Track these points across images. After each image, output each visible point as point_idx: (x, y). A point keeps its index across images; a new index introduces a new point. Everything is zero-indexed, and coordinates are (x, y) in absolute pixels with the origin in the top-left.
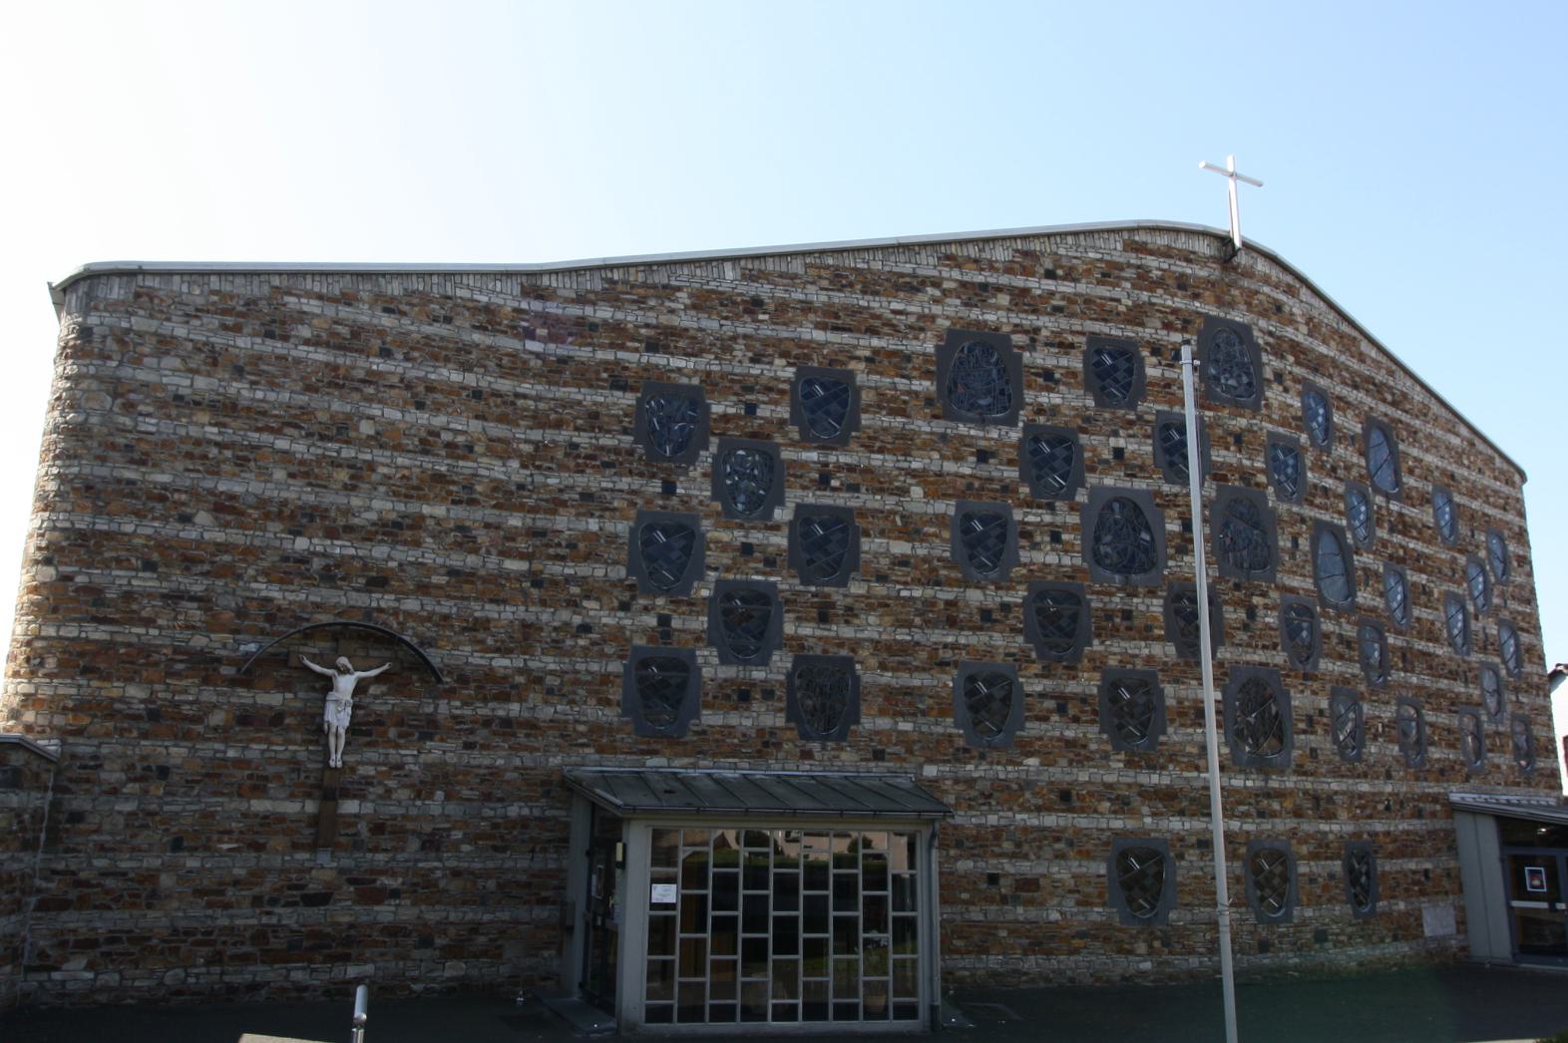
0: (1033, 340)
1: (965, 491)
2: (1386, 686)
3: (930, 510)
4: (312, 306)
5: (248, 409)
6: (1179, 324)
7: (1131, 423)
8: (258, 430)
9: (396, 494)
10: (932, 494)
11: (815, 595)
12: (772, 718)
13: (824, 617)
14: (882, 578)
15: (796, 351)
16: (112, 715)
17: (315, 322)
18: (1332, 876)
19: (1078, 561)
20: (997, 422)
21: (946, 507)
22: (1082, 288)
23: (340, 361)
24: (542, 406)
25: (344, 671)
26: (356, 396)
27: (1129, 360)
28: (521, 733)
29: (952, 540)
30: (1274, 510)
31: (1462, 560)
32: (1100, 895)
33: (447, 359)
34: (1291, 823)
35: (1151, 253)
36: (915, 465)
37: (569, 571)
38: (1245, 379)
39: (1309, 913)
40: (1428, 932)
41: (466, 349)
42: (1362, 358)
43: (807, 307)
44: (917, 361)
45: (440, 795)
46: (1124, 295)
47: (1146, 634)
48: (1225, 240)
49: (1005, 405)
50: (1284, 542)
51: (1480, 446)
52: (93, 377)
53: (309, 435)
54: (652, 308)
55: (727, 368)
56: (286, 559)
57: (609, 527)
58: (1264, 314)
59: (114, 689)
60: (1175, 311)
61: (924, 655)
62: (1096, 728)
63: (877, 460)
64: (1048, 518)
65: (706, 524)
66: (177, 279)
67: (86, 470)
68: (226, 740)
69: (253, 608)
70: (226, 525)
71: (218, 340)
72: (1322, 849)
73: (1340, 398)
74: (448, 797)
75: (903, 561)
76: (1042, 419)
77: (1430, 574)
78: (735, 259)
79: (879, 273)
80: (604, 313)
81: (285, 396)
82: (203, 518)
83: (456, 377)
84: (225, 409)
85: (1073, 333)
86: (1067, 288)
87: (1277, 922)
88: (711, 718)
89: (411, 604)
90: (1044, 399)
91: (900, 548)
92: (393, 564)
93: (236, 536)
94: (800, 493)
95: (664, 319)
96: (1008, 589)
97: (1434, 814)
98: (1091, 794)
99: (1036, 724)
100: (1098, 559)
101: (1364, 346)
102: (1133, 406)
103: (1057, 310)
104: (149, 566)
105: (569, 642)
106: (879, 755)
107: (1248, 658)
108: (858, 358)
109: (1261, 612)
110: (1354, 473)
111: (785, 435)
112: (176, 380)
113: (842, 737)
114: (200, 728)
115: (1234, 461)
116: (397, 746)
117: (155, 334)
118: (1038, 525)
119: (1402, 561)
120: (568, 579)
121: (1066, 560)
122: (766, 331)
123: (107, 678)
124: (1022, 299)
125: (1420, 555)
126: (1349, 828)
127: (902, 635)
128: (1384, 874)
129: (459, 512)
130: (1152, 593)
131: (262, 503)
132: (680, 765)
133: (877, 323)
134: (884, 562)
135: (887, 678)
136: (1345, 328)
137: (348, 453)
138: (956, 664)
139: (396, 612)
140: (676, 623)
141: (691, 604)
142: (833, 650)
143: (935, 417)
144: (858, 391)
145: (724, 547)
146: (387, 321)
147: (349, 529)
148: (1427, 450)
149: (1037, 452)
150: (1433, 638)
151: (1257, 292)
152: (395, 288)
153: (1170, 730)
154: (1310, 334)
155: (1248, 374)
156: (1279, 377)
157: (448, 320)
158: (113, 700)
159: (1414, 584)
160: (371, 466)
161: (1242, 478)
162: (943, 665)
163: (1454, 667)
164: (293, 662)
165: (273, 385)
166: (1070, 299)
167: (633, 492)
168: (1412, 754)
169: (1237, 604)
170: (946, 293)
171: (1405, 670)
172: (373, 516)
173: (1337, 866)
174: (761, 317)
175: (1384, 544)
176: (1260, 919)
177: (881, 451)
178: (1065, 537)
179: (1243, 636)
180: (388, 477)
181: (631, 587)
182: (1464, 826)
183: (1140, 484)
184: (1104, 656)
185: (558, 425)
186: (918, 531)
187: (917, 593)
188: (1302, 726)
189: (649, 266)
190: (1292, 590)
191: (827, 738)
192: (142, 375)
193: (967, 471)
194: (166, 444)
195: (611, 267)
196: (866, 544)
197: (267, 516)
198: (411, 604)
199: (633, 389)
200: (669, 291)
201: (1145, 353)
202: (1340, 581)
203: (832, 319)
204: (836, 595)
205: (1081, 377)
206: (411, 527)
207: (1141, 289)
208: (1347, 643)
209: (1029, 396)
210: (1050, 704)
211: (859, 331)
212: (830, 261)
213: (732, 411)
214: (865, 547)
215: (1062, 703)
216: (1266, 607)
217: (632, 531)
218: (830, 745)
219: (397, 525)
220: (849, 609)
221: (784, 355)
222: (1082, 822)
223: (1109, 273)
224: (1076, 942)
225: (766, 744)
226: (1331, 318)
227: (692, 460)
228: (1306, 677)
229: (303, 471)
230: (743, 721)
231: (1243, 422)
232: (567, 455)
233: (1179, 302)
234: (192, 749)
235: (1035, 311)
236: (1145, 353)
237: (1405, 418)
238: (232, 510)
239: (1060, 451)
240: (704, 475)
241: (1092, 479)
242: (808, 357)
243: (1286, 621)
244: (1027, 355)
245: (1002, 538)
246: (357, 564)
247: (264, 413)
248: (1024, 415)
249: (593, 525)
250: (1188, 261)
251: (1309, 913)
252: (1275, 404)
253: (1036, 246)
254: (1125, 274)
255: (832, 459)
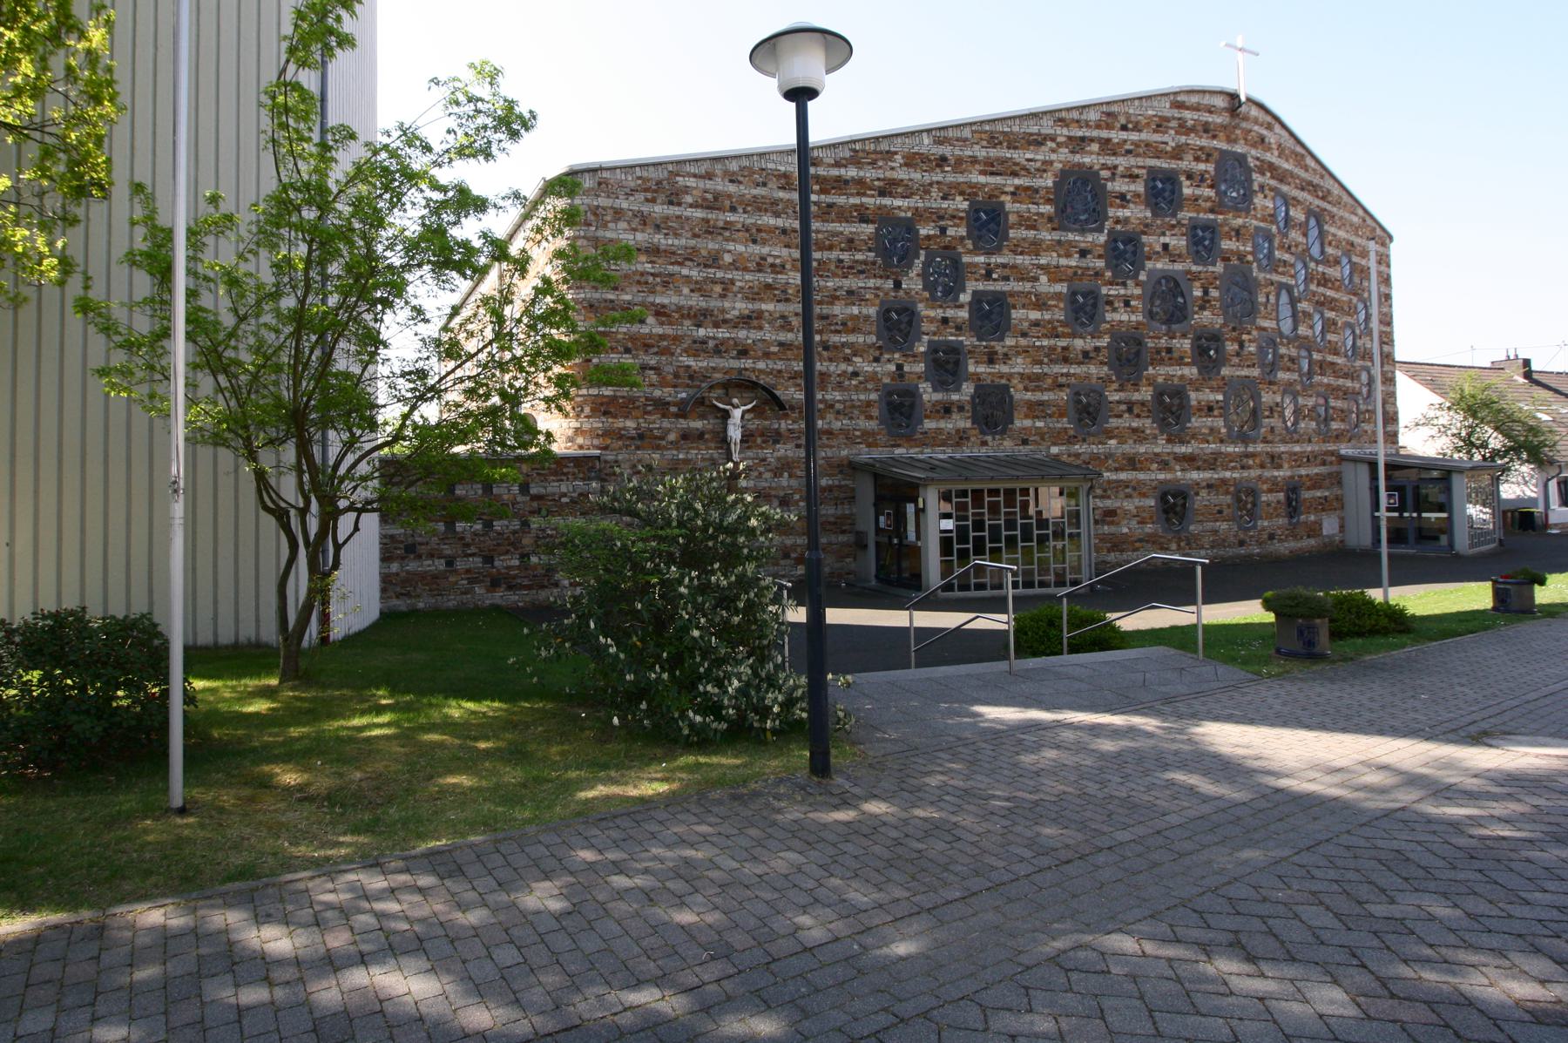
0: (1113, 174)
1: (1073, 276)
2: (1311, 385)
3: (1052, 290)
4: (691, 182)
5: (665, 251)
6: (1204, 157)
7: (1173, 226)
8: (672, 264)
9: (747, 298)
10: (1053, 280)
11: (985, 347)
12: (961, 422)
13: (991, 359)
14: (1024, 335)
15: (968, 191)
16: (621, 437)
17: (694, 192)
18: (1279, 502)
19: (1140, 318)
20: (1092, 231)
21: (1062, 288)
22: (1144, 136)
23: (710, 216)
24: (820, 236)
25: (736, 407)
26: (720, 238)
27: (1172, 184)
28: (824, 438)
29: (1065, 309)
30: (1256, 279)
31: (1355, 300)
32: (1151, 518)
33: (766, 210)
34: (1258, 472)
35: (1188, 108)
36: (1043, 262)
37: (844, 340)
38: (1242, 192)
39: (1266, 524)
40: (1325, 533)
41: (775, 202)
42: (1306, 168)
43: (974, 160)
44: (1042, 193)
45: (786, 474)
46: (1170, 139)
47: (1180, 362)
48: (1233, 96)
49: (1097, 218)
50: (1262, 299)
51: (1369, 221)
52: (584, 237)
53: (699, 265)
54: (880, 167)
55: (928, 205)
56: (695, 342)
57: (865, 311)
58: (1254, 146)
59: (620, 423)
60: (1202, 149)
61: (1049, 381)
62: (1150, 421)
63: (1019, 259)
64: (1122, 292)
65: (920, 306)
66: (618, 171)
67: (589, 296)
68: (677, 449)
69: (681, 371)
70: (662, 324)
71: (645, 209)
72: (1274, 486)
73: (1294, 198)
74: (790, 476)
75: (1036, 324)
76: (1119, 227)
77: (1337, 311)
78: (929, 131)
79: (1017, 134)
80: (852, 172)
81: (683, 241)
82: (651, 320)
83: (772, 221)
84: (654, 252)
85: (1139, 167)
86: (1134, 136)
87: (1249, 529)
88: (929, 424)
89: (761, 365)
90: (1121, 213)
91: (1035, 315)
92: (750, 341)
93: (668, 330)
94: (974, 283)
95: (889, 174)
96: (1099, 337)
97: (1331, 463)
98: (1146, 460)
99: (1114, 420)
100: (1151, 315)
101: (1309, 161)
102: (1174, 215)
103: (1129, 152)
104: (627, 351)
105: (847, 383)
106: (1025, 442)
107: (1238, 373)
108: (1006, 193)
109: (1247, 344)
110: (1300, 249)
111: (964, 246)
112: (626, 236)
113: (1003, 432)
114: (664, 443)
115: (1234, 248)
116: (762, 448)
117: (612, 208)
118: (1116, 296)
119: (1322, 304)
120: (844, 345)
121: (1133, 318)
122: (950, 178)
123: (615, 417)
124: (1107, 146)
125: (1333, 300)
126: (1289, 473)
127: (1037, 369)
128: (1305, 500)
129: (781, 307)
130: (1184, 336)
131: (679, 308)
132: (914, 452)
133: (1017, 168)
134: (1026, 324)
135: (1029, 396)
136: (1299, 149)
137: (720, 275)
138: (1068, 386)
139: (754, 370)
140: (906, 368)
141: (914, 356)
142: (997, 380)
143: (1054, 229)
144: (1007, 214)
145: (932, 320)
146: (732, 188)
147: (725, 321)
148: (1339, 228)
149: (1116, 249)
150: (1336, 353)
151: (1250, 131)
152: (734, 166)
153: (1193, 420)
154: (1279, 156)
155: (1244, 188)
156: (1262, 187)
157: (764, 184)
158: (620, 429)
159: (1329, 319)
160: (732, 282)
161: (1239, 259)
162: (1061, 386)
163: (1346, 370)
164: (707, 402)
165: (677, 235)
166: (1136, 144)
167: (877, 289)
168: (1322, 426)
169: (1233, 340)
170: (1059, 145)
171: (1321, 375)
172: (736, 313)
173: (1281, 496)
174: (947, 169)
175: (1314, 293)
176: (1240, 528)
177: (1022, 253)
178: (1132, 303)
179: (1236, 360)
180: (742, 288)
181: (880, 348)
182: (1347, 468)
183: (1178, 267)
184: (1155, 377)
185: (830, 248)
186: (1045, 304)
187: (1045, 343)
188: (1267, 413)
189: (877, 139)
190: (1264, 329)
191: (996, 433)
192: (609, 235)
193: (1073, 263)
194: (626, 276)
195: (854, 142)
196: (1015, 314)
197: (682, 316)
198: (761, 365)
199: (873, 222)
200: (890, 154)
201: (1183, 178)
202: (1290, 321)
203: (990, 167)
204: (998, 347)
205: (1143, 197)
206: (757, 318)
207: (1181, 134)
208: (1292, 360)
209: (1111, 212)
210: (1124, 407)
211: (1006, 174)
212: (987, 128)
213: (932, 232)
214: (1014, 316)
215: (1130, 406)
216: (1250, 341)
217: (878, 313)
218: (997, 437)
219: (749, 317)
220: (1006, 355)
221: (962, 193)
222: (1141, 476)
223: (1161, 125)
224: (1137, 545)
225: (961, 438)
226: (1290, 143)
227: (910, 266)
228: (1271, 383)
229: (699, 288)
230: (948, 425)
231: (1240, 221)
232: (837, 267)
233: (1204, 142)
234: (662, 455)
235: (1114, 154)
236: (1183, 178)
237: (1329, 207)
238: (664, 314)
239: (1130, 248)
240: (918, 275)
241: (1149, 265)
242: (976, 194)
243: (1260, 348)
244: (1109, 184)
245: (1095, 306)
246: (732, 342)
247: (674, 253)
248: (1108, 225)
249: (855, 310)
250: (1211, 112)
251: (1266, 524)
252: (1259, 207)
253: (1115, 108)
254: (1171, 125)
255: (993, 260)
